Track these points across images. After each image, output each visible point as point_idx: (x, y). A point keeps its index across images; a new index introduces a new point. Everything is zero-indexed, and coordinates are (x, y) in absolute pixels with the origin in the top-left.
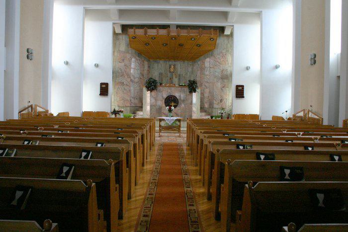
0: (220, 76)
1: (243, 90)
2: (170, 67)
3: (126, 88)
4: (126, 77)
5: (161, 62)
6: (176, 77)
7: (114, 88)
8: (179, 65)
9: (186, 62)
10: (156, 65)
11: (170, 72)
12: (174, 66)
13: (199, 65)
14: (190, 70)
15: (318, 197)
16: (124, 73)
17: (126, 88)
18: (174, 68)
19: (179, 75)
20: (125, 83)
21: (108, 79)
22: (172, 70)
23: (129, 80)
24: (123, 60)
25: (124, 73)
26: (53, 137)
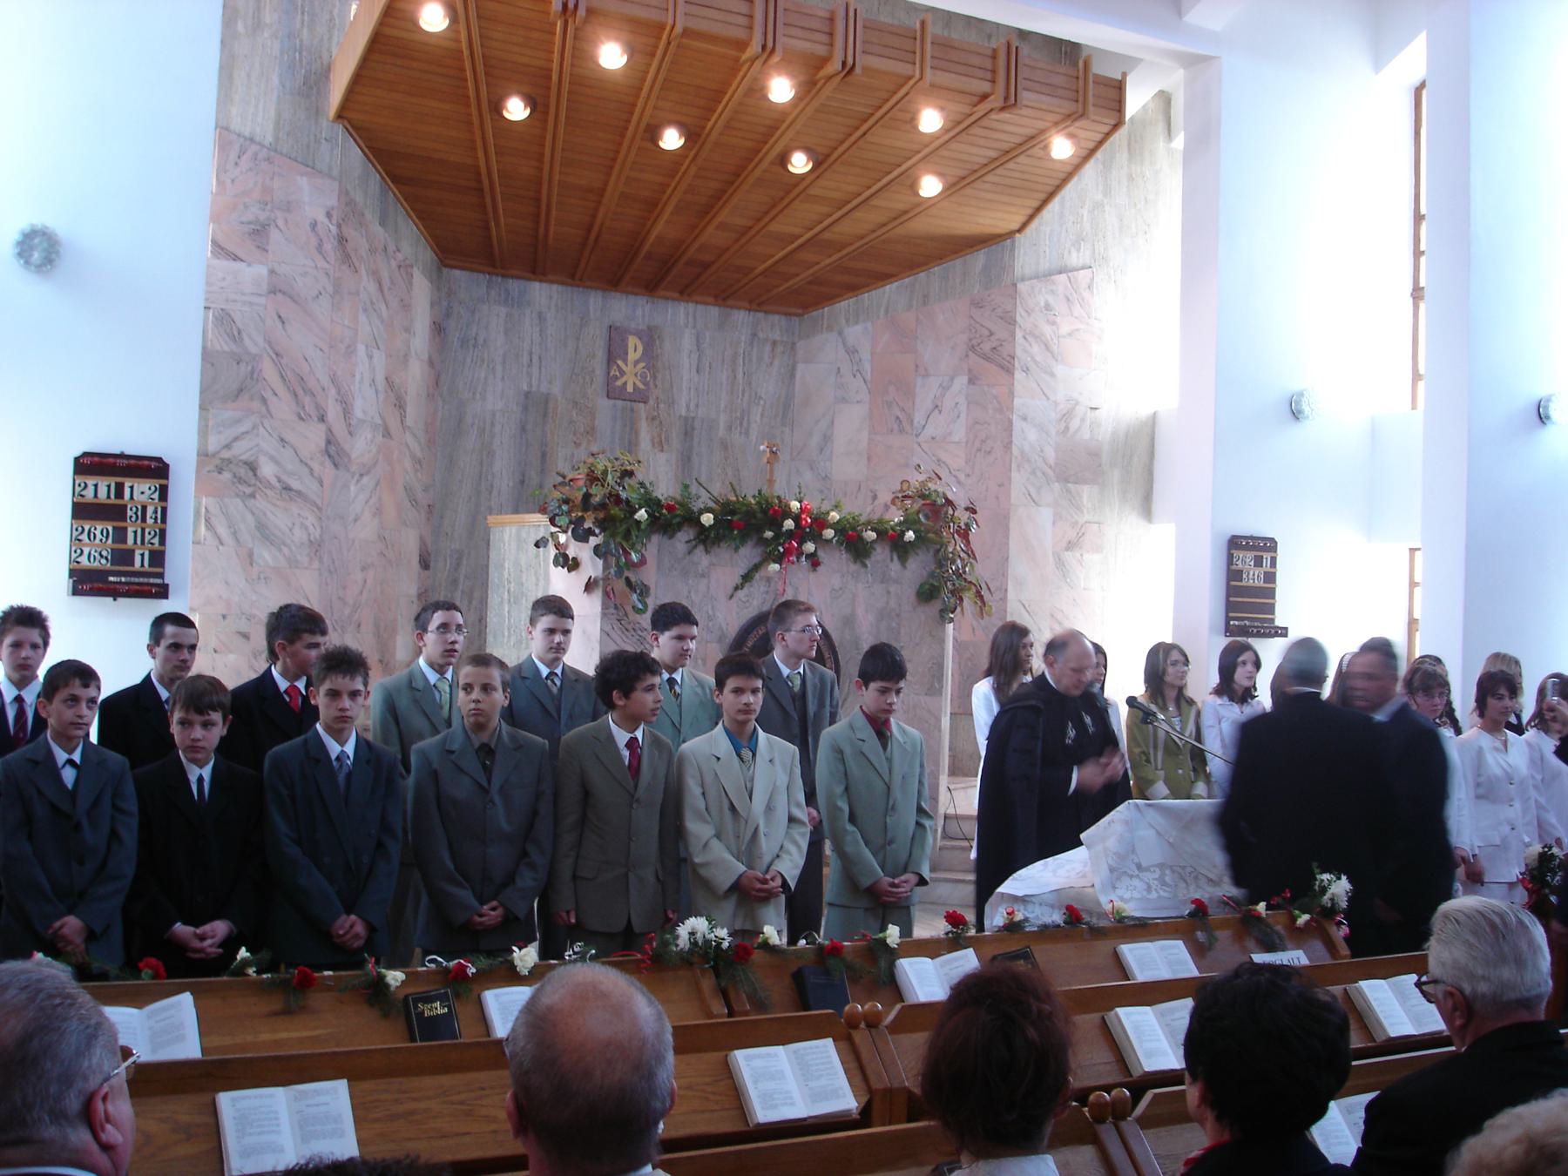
0: (1050, 454)
1: (1271, 593)
2: (615, 352)
3: (279, 519)
4: (283, 407)
5: (542, 294)
6: (660, 444)
7: (202, 486)
8: (687, 341)
9: (741, 317)
10: (494, 318)
11: (613, 392)
12: (650, 338)
13: (852, 351)
14: (768, 385)
15: (510, 1025)
16: (269, 371)
17: (279, 519)
18: (650, 355)
19: (688, 432)
20: (267, 470)
21: (156, 416)
22: (631, 382)
23: (313, 437)
24: (259, 233)
25: (269, 371)
26: (1088, 720)
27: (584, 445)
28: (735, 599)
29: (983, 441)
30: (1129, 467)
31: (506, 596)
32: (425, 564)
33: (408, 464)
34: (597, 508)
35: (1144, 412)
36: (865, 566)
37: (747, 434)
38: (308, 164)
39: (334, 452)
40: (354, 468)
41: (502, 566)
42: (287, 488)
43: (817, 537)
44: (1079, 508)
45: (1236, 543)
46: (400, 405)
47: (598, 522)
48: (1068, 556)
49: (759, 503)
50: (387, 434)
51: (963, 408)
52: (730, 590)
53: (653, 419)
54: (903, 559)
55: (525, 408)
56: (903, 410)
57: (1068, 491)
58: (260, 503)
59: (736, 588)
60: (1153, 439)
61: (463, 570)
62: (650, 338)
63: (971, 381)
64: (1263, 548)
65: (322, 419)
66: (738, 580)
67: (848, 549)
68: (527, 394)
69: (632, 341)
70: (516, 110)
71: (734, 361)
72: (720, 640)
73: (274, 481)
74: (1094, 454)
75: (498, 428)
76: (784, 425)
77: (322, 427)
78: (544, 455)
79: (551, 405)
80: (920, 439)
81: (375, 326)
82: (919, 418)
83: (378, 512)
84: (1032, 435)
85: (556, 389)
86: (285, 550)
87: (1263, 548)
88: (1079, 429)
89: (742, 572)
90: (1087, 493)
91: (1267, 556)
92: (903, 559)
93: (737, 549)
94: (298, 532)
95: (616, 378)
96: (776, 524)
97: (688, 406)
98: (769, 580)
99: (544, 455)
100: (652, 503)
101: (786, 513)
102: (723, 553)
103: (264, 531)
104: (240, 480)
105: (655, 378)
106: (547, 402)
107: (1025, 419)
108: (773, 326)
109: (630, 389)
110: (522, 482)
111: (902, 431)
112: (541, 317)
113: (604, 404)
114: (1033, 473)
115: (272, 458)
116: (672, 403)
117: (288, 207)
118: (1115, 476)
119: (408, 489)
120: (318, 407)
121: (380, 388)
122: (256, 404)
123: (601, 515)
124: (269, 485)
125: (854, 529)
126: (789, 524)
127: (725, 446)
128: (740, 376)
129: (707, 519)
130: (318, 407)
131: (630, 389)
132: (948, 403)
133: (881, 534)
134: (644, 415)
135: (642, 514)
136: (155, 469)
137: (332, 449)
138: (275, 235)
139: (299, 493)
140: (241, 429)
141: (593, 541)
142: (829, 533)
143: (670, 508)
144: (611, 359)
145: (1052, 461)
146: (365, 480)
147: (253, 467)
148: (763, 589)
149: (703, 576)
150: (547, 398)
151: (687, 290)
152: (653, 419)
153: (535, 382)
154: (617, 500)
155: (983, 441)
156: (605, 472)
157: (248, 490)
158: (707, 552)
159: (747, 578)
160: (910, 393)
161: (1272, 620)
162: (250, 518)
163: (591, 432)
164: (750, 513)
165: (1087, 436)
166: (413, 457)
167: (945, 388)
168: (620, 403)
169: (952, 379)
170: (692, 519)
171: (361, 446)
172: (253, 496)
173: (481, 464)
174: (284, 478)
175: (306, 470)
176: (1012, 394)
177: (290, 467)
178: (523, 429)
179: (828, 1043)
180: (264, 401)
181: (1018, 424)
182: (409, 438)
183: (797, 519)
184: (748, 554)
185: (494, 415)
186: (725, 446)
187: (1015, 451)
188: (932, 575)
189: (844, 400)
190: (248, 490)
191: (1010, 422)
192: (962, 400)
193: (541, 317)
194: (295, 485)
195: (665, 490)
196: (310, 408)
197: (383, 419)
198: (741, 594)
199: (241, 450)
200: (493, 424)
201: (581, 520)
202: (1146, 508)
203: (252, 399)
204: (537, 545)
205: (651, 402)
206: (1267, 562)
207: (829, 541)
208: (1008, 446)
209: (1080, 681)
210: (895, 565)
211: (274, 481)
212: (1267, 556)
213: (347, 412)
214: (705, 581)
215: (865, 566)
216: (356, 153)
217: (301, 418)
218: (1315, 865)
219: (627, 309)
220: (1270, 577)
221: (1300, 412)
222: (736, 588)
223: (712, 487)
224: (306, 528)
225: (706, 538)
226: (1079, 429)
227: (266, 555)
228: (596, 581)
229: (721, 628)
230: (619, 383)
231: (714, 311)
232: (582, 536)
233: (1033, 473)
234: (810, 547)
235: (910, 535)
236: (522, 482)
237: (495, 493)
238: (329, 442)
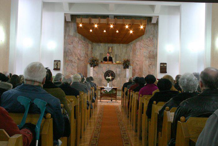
2: (109, 49)
4: (74, 56)
5: (102, 44)
8: (116, 47)
9: (121, 45)
12: (112, 47)
14: (124, 51)
16: (73, 53)
18: (112, 49)
20: (73, 61)
25: (73, 53)
38: (76, 37)
50: (85, 57)
62: (112, 47)
69: (110, 48)
70: (105, 31)
71: (121, 49)
81: (80, 48)
103: (73, 65)
108: (125, 45)
112: (102, 46)
117: (74, 40)
127: (120, 57)
136: (60, 61)
138: (73, 43)
144: (108, 49)
147: (72, 61)
151: (115, 43)
179: (156, 23)
186: (120, 57)
193: (102, 46)
199: (71, 59)
204: (111, 59)
209: (185, 117)
216: (80, 35)
219: (110, 45)
227: (73, 67)
231: (119, 44)
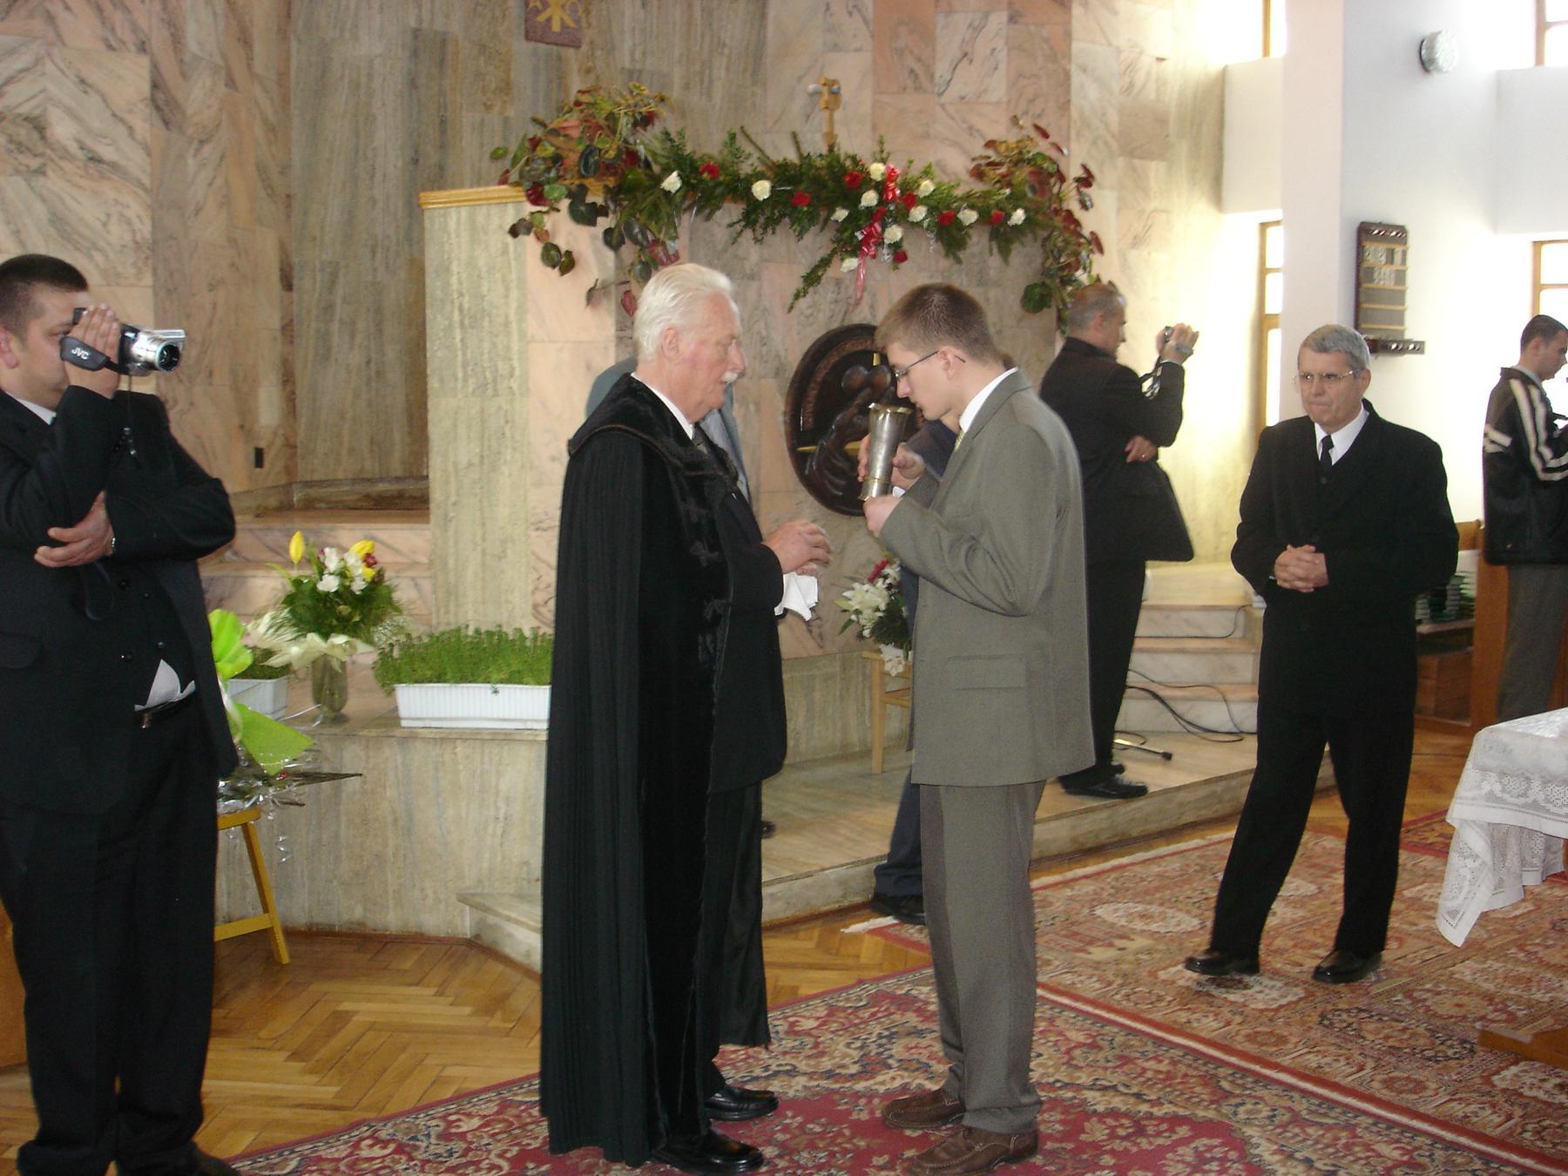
0: (1114, 118)
11: (534, 32)
20: (62, 130)
27: (496, 109)
28: (794, 312)
29: (1031, 101)
30: (1197, 135)
31: (456, 316)
32: (287, 283)
33: (259, 131)
34: (609, 168)
35: (1214, 67)
36: (959, 261)
37: (709, 96)
39: (163, 103)
40: (190, 131)
41: (448, 270)
42: (95, 159)
43: (901, 218)
44: (1145, 191)
45: (1365, 232)
46: (246, 41)
47: (613, 194)
48: (1133, 254)
49: (830, 166)
50: (231, 82)
51: (1002, 55)
52: (790, 300)
53: (588, 71)
54: (1005, 253)
55: (415, 54)
56: (919, 60)
57: (1134, 169)
58: (53, 183)
59: (797, 296)
60: (1222, 103)
61: (340, 291)
63: (1012, 19)
64: (1394, 235)
65: (143, 48)
66: (798, 284)
67: (940, 237)
68: (416, 33)
72: (777, 373)
73: (73, 148)
74: (1162, 120)
75: (377, 83)
76: (754, 83)
77: (145, 61)
78: (443, 122)
79: (450, 48)
80: (943, 99)
82: (941, 69)
83: (226, 202)
84: (1093, 93)
85: (456, 27)
86: (99, 257)
87: (1394, 235)
88: (1144, 85)
89: (804, 271)
90: (1155, 169)
91: (1398, 249)
92: (1005, 253)
93: (800, 236)
94: (115, 229)
95: (538, 12)
96: (852, 200)
97: (632, 54)
98: (838, 282)
99: (443, 122)
100: (689, 168)
101: (860, 181)
102: (782, 240)
104: (21, 147)
105: (587, 12)
106: (444, 42)
107: (1084, 70)
109: (556, 27)
110: (416, 161)
111: (918, 88)
113: (522, 49)
114: (1094, 143)
115: (70, 112)
116: (611, 50)
118: (1183, 148)
119: (262, 170)
120: (135, 29)
121: (220, 12)
122: (38, 25)
123: (611, 182)
124: (66, 155)
125: (948, 207)
126: (870, 198)
128: (697, 13)
129: (762, 190)
130: (135, 29)
131: (556, 27)
132: (981, 49)
133: (986, 218)
134: (575, 67)
135: (672, 182)
137: (160, 96)
139: (114, 166)
140: (19, 63)
141: (604, 223)
142: (919, 213)
143: (712, 170)
145: (1115, 127)
146: (207, 149)
147: (38, 126)
148: (831, 296)
149: (752, 277)
150: (443, 40)
152: (588, 71)
153: (426, 16)
154: (632, 156)
155: (1031, 101)
156: (612, 117)
157: (35, 163)
158: (757, 241)
159: (812, 279)
160: (926, 35)
161: (1402, 332)
162: (39, 208)
163: (506, 88)
164: (817, 181)
165: (1152, 97)
166: (265, 121)
167: (976, 29)
168: (542, 47)
169: (986, 16)
170: (739, 189)
171: (199, 96)
172: (41, 172)
173: (358, 137)
174: (89, 142)
175: (121, 128)
176: (1068, 36)
177: (97, 125)
178: (413, 84)
180: (50, 18)
181: (1077, 78)
182: (258, 91)
183: (881, 188)
184: (816, 243)
185: (371, 61)
187: (1074, 114)
188: (1045, 272)
189: (836, 47)
190: (35, 163)
191: (1067, 75)
192: (1000, 43)
194: (107, 153)
195: (707, 144)
196: (124, 32)
197: (224, 56)
198: (803, 303)
200: (370, 76)
201: (583, 190)
202: (1217, 192)
203: (31, 16)
205: (584, 48)
206: (1398, 258)
207: (919, 224)
208: (1065, 105)
210: (995, 261)
211: (73, 148)
212: (1398, 249)
213: (177, 41)
214: (755, 284)
215: (959, 261)
217: (110, 47)
218: (102, 495)
220: (1401, 277)
221: (1432, 61)
222: (797, 296)
223: (784, 133)
224: (129, 223)
225: (756, 217)
226: (1144, 85)
228: (605, 287)
229: (778, 356)
230: (542, 18)
232: (585, 215)
233: (1094, 143)
234: (894, 233)
235: (1019, 216)
236: (416, 161)
237: (378, 177)
238: (155, 86)
